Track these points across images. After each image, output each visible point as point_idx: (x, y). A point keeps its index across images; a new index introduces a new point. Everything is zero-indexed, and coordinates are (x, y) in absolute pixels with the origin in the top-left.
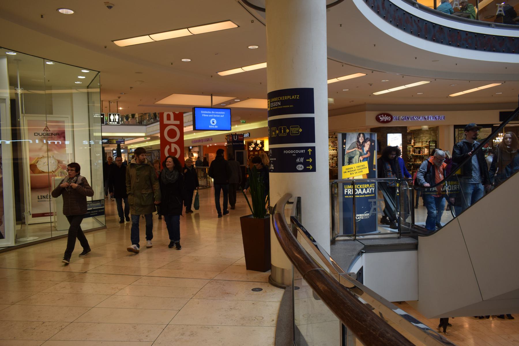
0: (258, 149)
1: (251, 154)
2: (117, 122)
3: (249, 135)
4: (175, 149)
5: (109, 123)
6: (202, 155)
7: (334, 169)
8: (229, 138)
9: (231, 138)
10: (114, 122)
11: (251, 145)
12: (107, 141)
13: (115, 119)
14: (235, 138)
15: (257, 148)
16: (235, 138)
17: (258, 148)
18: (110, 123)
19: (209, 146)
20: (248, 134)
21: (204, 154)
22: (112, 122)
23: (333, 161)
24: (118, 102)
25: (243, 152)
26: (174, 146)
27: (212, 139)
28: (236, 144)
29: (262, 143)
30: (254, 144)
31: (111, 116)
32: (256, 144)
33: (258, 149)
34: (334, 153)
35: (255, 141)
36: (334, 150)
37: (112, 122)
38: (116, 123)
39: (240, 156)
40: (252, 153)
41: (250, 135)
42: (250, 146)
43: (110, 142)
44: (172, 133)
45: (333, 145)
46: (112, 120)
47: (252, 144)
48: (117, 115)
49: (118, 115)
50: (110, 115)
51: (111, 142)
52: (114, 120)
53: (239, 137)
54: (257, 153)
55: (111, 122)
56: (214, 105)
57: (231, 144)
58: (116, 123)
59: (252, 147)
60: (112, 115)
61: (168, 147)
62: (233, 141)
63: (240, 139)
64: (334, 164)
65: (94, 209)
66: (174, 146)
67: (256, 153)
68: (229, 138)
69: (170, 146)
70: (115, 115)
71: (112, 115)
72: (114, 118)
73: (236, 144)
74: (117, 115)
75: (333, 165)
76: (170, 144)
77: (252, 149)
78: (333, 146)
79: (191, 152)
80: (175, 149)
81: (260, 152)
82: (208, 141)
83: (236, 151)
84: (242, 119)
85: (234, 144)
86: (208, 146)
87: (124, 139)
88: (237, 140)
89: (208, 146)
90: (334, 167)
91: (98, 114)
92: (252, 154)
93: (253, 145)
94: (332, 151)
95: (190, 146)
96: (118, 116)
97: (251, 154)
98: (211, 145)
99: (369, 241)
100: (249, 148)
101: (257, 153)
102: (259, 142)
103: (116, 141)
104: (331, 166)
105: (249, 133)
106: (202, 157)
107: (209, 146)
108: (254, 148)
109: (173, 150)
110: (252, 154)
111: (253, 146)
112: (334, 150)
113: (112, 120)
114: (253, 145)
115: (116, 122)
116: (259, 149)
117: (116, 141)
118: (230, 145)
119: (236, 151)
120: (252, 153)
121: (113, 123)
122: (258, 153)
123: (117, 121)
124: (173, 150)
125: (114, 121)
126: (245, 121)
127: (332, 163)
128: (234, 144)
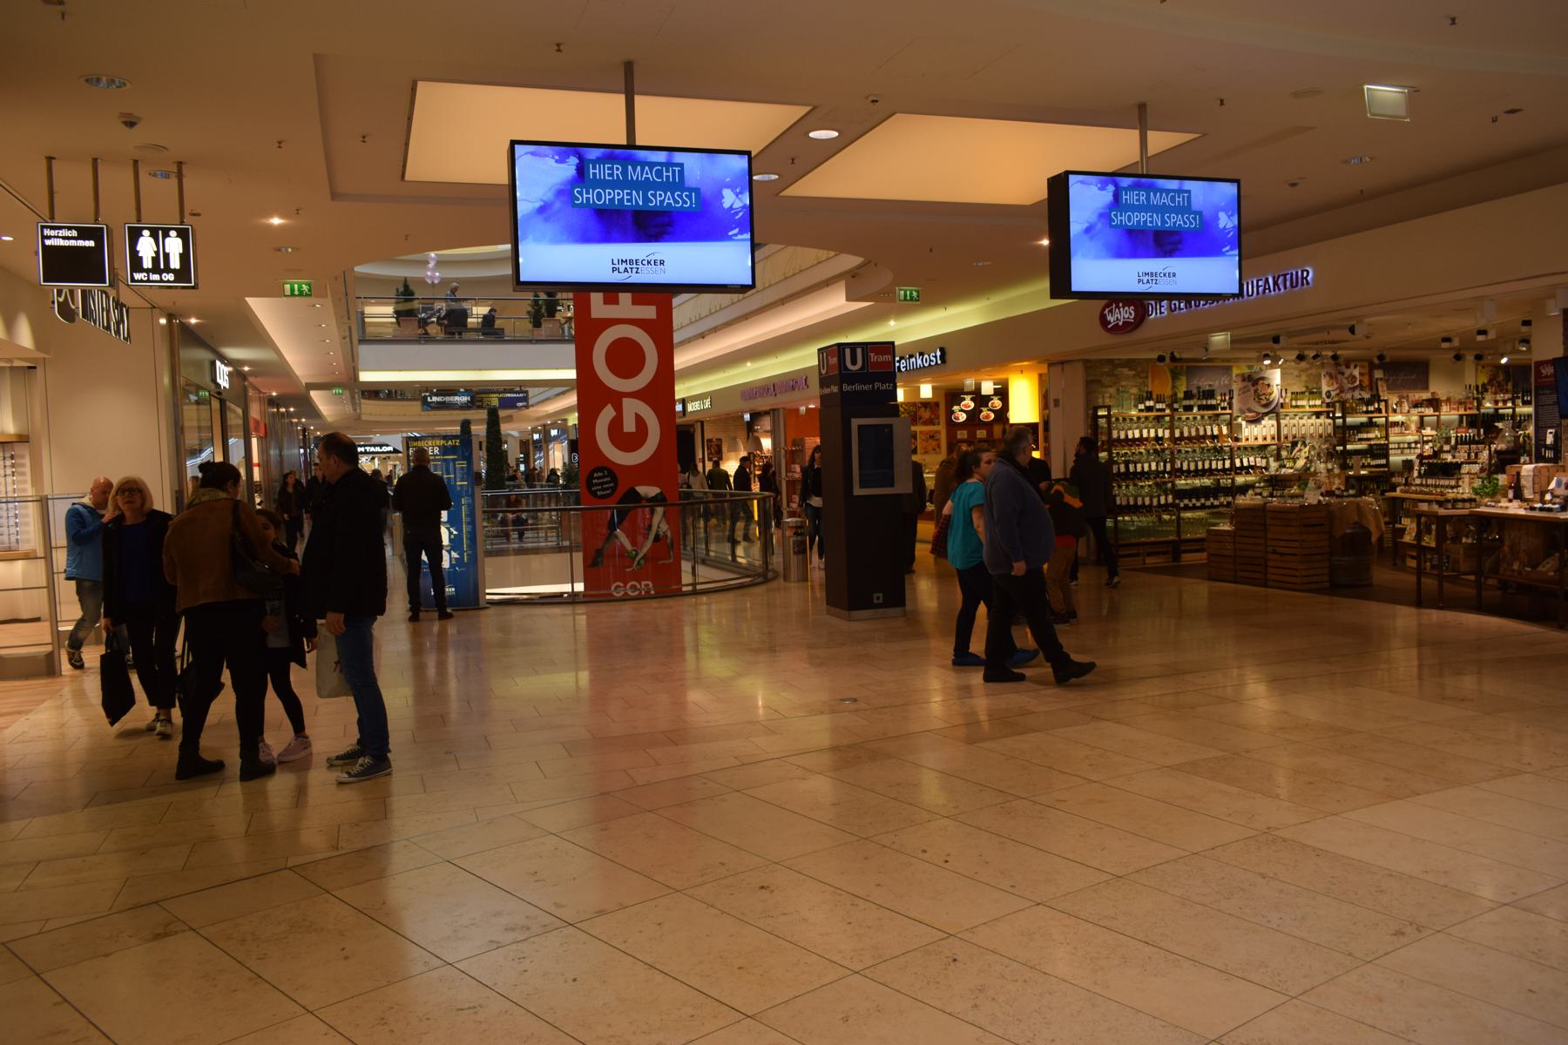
0: (988, 416)
1: (959, 437)
2: (174, 271)
3: (942, 357)
4: (640, 421)
5: (133, 280)
6: (783, 445)
7: (1341, 503)
8: (827, 360)
9: (834, 360)
10: (160, 272)
11: (959, 401)
12: (469, 399)
13: (167, 256)
14: (854, 362)
15: (985, 412)
16: (854, 362)
17: (987, 415)
18: (138, 276)
19: (808, 410)
20: (938, 353)
21: (790, 440)
22: (148, 271)
23: (1330, 466)
24: (184, 168)
25: (890, 426)
26: (632, 407)
27: (808, 383)
28: (858, 387)
29: (1003, 393)
30: (972, 399)
31: (141, 239)
32: (981, 400)
33: (988, 416)
34: (1321, 430)
35: (970, 383)
36: (1318, 417)
37: (148, 271)
38: (171, 277)
39: (880, 449)
40: (965, 432)
41: (948, 357)
42: (956, 408)
43: (479, 401)
44: (625, 358)
45: (1336, 386)
46: (147, 264)
47: (964, 399)
48: (173, 233)
49: (182, 234)
50: (135, 235)
51: (481, 401)
52: (155, 260)
53: (873, 357)
54: (984, 432)
55: (142, 270)
56: (839, 284)
57: (835, 389)
58: (171, 277)
59: (962, 411)
60: (146, 233)
61: (608, 413)
62: (845, 376)
63: (878, 364)
64: (1337, 481)
65: (756, 518)
66: (632, 407)
67: (981, 434)
68: (827, 360)
69: (619, 409)
70: (166, 235)
71: (146, 233)
72: (157, 253)
73: (858, 387)
74: (173, 233)
75: (1332, 483)
76: (616, 398)
77: (962, 417)
78: (1333, 394)
79: (756, 434)
80: (640, 421)
81: (997, 429)
82: (793, 388)
83: (856, 422)
84: (900, 280)
85: (846, 387)
86: (803, 409)
87: (527, 392)
88: (862, 368)
89: (803, 409)
90: (1338, 496)
91: (70, 228)
92: (966, 437)
93: (969, 403)
94: (1309, 418)
95: (746, 412)
96: (179, 241)
97: (959, 437)
98: (812, 406)
99: (798, 288)
100: (953, 412)
101: (984, 432)
102: (988, 388)
103: (500, 399)
104: (1323, 490)
105: (942, 350)
106: (783, 452)
107: (808, 410)
108: (973, 415)
109: (629, 426)
110: (966, 437)
111: (966, 406)
112: (1318, 415)
113: (147, 264)
114: (969, 403)
115: (168, 269)
116: (992, 416)
117: (500, 399)
118: (832, 394)
119: (856, 422)
120: (965, 432)
121: (156, 277)
122: (990, 433)
123: (175, 263)
124: (629, 426)
125: (156, 269)
126: (918, 292)
127: (1328, 477)
128: (846, 387)
